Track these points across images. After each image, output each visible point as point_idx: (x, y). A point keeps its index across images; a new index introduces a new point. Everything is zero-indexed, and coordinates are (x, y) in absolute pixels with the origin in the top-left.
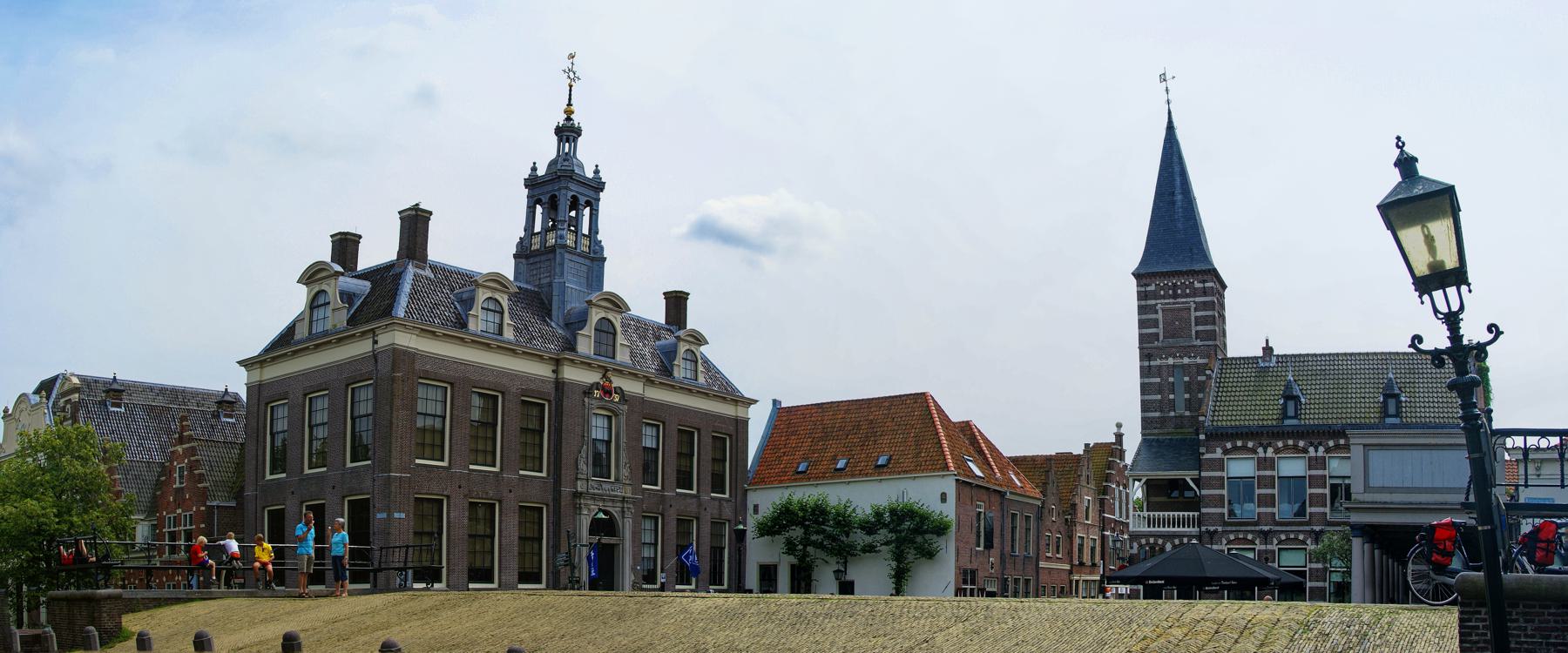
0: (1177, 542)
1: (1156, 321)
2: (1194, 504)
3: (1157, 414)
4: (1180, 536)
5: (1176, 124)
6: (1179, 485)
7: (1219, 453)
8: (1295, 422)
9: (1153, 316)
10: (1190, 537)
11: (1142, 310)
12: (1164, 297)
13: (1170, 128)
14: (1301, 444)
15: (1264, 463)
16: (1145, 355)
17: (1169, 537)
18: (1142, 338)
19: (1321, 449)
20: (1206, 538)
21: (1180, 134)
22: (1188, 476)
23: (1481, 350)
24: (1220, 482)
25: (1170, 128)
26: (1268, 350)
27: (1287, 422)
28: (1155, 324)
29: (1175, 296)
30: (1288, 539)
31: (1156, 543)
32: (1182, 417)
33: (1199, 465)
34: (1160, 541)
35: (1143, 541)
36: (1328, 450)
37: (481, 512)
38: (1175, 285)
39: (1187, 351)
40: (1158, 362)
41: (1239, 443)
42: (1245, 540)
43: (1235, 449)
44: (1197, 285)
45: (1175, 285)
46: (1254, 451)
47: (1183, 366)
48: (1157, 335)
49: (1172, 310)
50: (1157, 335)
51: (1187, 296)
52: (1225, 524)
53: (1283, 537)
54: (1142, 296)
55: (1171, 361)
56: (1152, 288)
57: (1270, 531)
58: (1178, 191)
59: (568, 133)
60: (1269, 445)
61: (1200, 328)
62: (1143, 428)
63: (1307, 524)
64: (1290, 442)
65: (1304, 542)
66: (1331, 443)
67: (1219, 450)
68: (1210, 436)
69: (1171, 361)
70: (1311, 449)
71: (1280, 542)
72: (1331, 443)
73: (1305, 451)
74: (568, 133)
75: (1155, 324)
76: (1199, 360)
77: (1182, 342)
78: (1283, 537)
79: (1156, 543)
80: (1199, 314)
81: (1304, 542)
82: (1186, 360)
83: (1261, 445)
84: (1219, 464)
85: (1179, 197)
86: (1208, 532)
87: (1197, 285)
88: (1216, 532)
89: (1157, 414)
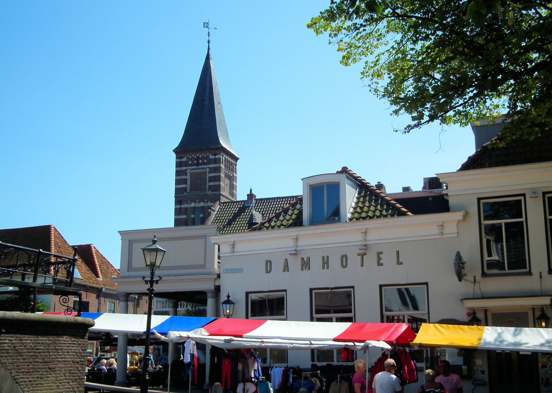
1: (186, 180)
5: (211, 56)
9: (184, 177)
11: (178, 173)
12: (191, 165)
13: (208, 58)
16: (178, 201)
18: (177, 191)
23: (391, 67)
25: (208, 58)
28: (185, 181)
29: (197, 164)
38: (198, 158)
44: (212, 157)
45: (198, 158)
51: (206, 164)
54: (178, 165)
55: (193, 205)
56: (184, 160)
59: (251, 190)
69: (193, 205)
74: (251, 190)
75: (185, 181)
77: (201, 193)
80: (211, 175)
85: (207, 102)
87: (212, 157)
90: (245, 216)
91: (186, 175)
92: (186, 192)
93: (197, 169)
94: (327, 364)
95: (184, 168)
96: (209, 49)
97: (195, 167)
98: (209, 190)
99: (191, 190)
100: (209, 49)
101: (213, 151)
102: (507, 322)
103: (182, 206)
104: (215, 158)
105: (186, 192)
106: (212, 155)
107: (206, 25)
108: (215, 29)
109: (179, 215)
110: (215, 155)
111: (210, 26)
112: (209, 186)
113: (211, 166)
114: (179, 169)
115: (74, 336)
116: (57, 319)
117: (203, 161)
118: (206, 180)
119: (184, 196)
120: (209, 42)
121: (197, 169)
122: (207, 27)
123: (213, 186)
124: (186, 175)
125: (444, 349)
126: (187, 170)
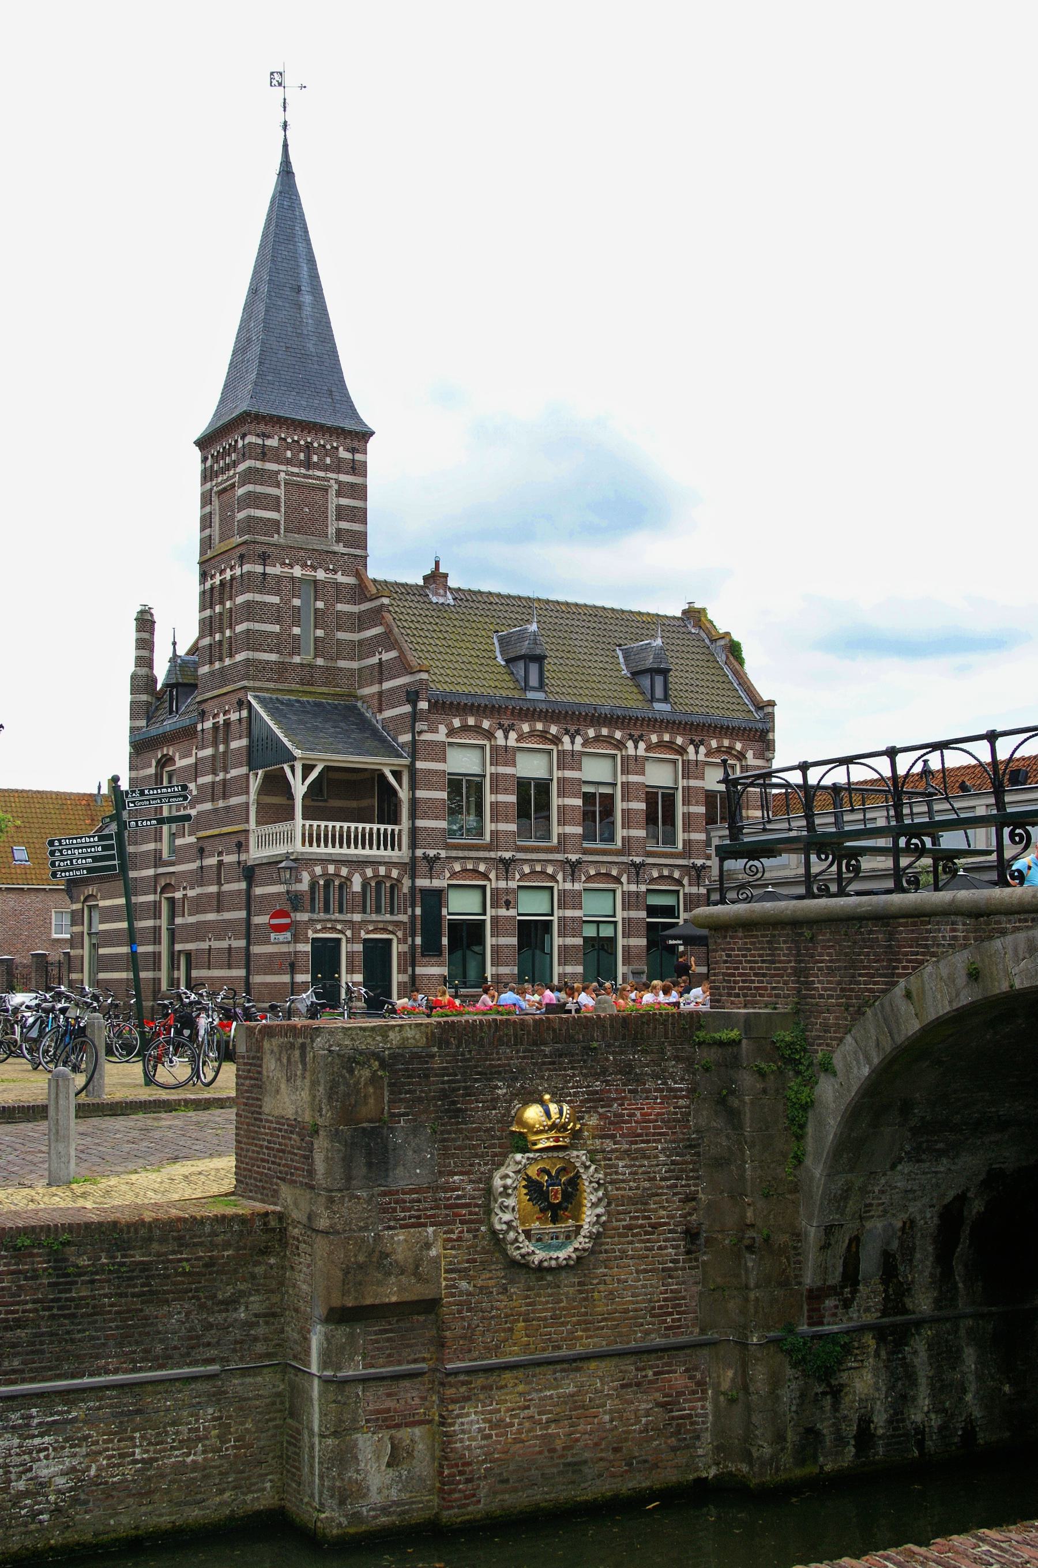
2: (389, 813)
3: (273, 657)
4: (375, 863)
5: (296, 168)
7: (441, 735)
8: (540, 696)
10: (389, 864)
12: (289, 462)
13: (286, 172)
14: (554, 730)
20: (422, 867)
25: (286, 172)
26: (436, 578)
27: (531, 695)
28: (342, 513)
29: (308, 464)
30: (533, 872)
34: (344, 871)
35: (382, 870)
37: (590, 815)
38: (308, 446)
39: (322, 558)
41: (471, 721)
44: (343, 454)
45: (308, 446)
49: (298, 485)
50: (277, 523)
51: (327, 468)
53: (527, 870)
56: (273, 442)
57: (513, 860)
59: (437, 563)
61: (344, 525)
63: (489, 848)
65: (617, 880)
66: (526, 728)
67: (443, 729)
73: (556, 740)
74: (437, 563)
75: (342, 513)
78: (527, 870)
86: (426, 857)
87: (343, 454)
88: (437, 858)
89: (273, 657)
94: (486, 978)
97: (303, 471)
98: (338, 541)
100: (285, 146)
101: (348, 441)
103: (269, 570)
107: (277, 79)
110: (353, 451)
113: (344, 478)
116: (842, 906)
122: (280, 84)
126: (278, 472)
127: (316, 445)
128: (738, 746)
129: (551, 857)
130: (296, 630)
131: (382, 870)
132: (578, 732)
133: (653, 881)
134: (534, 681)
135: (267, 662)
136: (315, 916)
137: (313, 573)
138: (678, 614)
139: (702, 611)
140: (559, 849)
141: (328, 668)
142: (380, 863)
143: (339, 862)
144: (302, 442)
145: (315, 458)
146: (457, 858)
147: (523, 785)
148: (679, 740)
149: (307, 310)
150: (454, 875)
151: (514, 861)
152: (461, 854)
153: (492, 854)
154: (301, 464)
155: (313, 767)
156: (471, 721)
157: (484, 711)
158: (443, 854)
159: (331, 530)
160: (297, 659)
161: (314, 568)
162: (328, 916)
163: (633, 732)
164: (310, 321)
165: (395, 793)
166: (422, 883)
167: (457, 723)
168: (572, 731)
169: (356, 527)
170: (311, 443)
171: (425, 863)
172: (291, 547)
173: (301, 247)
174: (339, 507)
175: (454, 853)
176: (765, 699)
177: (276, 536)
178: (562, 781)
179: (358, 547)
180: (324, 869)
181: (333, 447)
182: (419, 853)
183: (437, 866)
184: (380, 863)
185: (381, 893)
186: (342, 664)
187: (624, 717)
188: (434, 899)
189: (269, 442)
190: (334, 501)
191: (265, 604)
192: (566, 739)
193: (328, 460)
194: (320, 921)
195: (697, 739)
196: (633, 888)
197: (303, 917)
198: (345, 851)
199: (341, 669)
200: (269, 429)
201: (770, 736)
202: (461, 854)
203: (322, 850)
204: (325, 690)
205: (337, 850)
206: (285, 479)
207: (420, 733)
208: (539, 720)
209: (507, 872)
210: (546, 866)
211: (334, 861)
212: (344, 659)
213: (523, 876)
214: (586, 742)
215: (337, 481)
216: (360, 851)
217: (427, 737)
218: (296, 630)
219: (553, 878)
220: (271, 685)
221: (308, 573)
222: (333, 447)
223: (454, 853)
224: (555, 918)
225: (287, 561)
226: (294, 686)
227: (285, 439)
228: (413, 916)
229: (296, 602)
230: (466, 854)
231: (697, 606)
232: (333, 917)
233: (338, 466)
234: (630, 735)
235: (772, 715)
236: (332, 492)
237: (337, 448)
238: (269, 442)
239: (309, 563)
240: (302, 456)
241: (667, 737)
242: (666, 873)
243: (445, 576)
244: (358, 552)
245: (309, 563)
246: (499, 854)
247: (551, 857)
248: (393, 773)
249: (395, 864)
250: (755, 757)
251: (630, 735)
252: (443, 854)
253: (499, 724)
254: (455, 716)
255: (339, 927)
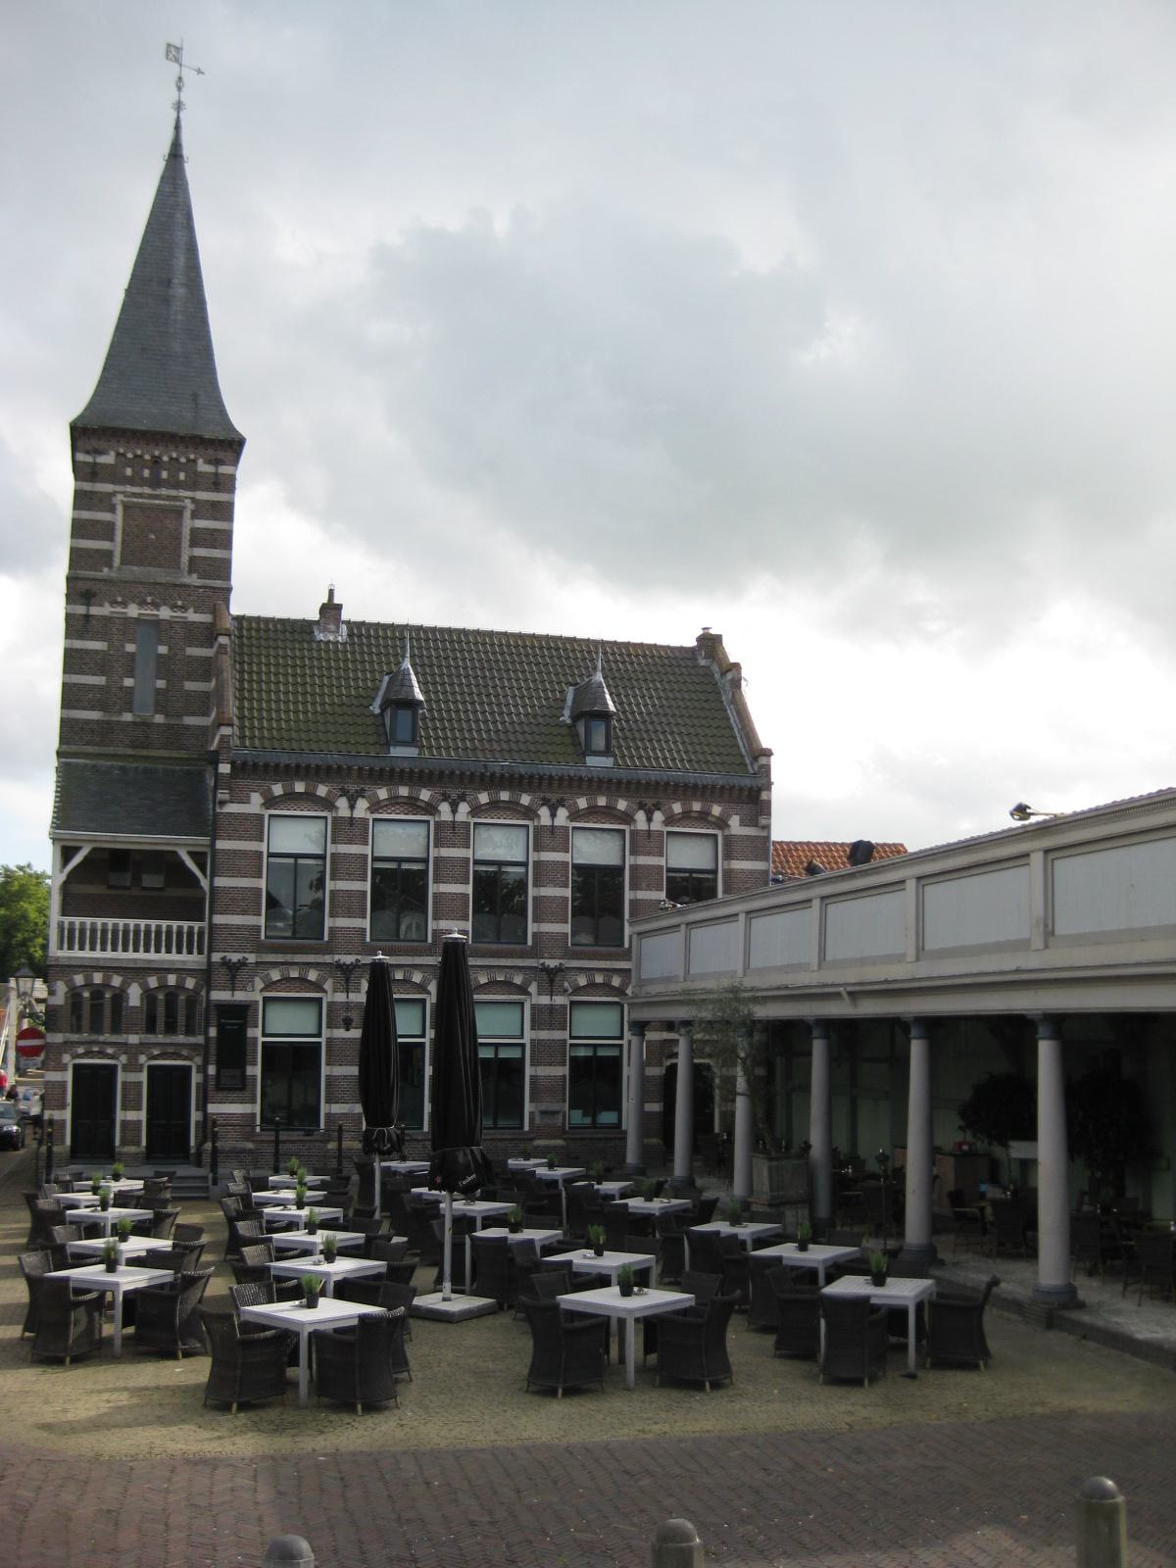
0: (153, 982)
2: (192, 909)
3: (94, 715)
4: (162, 971)
5: (187, 151)
6: (167, 863)
7: (255, 804)
8: (412, 752)
12: (131, 481)
13: (175, 156)
14: (425, 795)
15: (544, 838)
17: (137, 972)
19: (658, 816)
20: (220, 976)
21: (191, 170)
22: (183, 846)
24: (251, 863)
25: (175, 156)
26: (331, 609)
28: (107, 530)
29: (155, 482)
31: (106, 985)
32: (145, 725)
33: (212, 827)
35: (79, 980)
36: (476, 810)
39: (168, 593)
40: (106, 610)
42: (508, 985)
43: (290, 797)
44: (203, 467)
45: (156, 461)
46: (328, 804)
47: (157, 623)
48: (109, 554)
50: (109, 554)
51: (178, 485)
52: (260, 948)
56: (108, 459)
57: (560, 969)
58: (178, 279)
59: (331, 593)
60: (361, 794)
61: (200, 552)
62: (64, 739)
64: (404, 791)
65: (523, 990)
66: (677, 808)
67: (256, 799)
68: (240, 769)
69: (133, 611)
70: (445, 807)
71: (270, 985)
72: (677, 808)
74: (331, 593)
75: (198, 538)
76: (192, 616)
79: (106, 985)
81: (317, 986)
82: (165, 613)
83: (344, 793)
84: (254, 827)
86: (225, 963)
87: (203, 467)
88: (243, 964)
89: (94, 715)
90: (1053, 863)
91: (112, 509)
92: (110, 566)
93: (151, 497)
95: (108, 488)
96: (177, 127)
97: (147, 490)
98: (190, 572)
99: (123, 562)
100: (177, 127)
102: (89, 1291)
103: (95, 611)
104: (216, 474)
105: (110, 566)
106: (209, 462)
107: (174, 53)
108: (199, 72)
109: (82, 638)
110: (217, 462)
111: (185, 59)
112: (192, 559)
113: (202, 495)
114: (87, 486)
115: (147, 1024)
117: (173, 475)
118: (178, 538)
119: (104, 581)
120: (179, 106)
121: (151, 497)
123: (205, 558)
124: (112, 509)
125: (855, 869)
126: (114, 494)
127: (165, 459)
128: (716, 810)
129: (419, 960)
130: (128, 682)
131: (172, 980)
132: (462, 797)
133: (577, 990)
134: (404, 733)
135: (87, 722)
136: (152, 1038)
137: (184, 615)
138: (693, 643)
139: (718, 639)
140: (535, 952)
141: (170, 727)
142: (169, 971)
143: (108, 969)
144: (147, 457)
145: (164, 475)
146: (581, 970)
147: (584, 871)
148: (622, 805)
149: (177, 306)
150: (270, 985)
151: (359, 967)
152: (280, 958)
153: (328, 959)
154: (143, 482)
155: (77, 849)
156: (300, 787)
157: (580, 786)
158: (252, 958)
159: (185, 559)
160: (128, 717)
161: (156, 606)
162: (94, 1037)
163: (548, 795)
164: (180, 317)
165: (197, 880)
166: (220, 996)
167: (278, 789)
168: (454, 796)
169: (216, 553)
170: (159, 457)
171: (224, 970)
172: (126, 582)
173: (180, 237)
174: (194, 531)
175: (271, 958)
176: (764, 747)
177: (106, 570)
178: (634, 868)
179: (219, 578)
180: (107, 978)
181: (189, 460)
182: (216, 957)
183: (243, 974)
184: (169, 971)
185: (168, 1010)
186: (189, 720)
187: (531, 777)
188: (237, 1016)
189: (102, 459)
190: (188, 524)
191: (87, 652)
192: (445, 807)
193: (182, 476)
194: (81, 1043)
195: (649, 802)
196: (545, 1000)
197: (57, 1038)
198: (120, 955)
199: (187, 727)
200: (102, 444)
201: (764, 796)
202: (280, 958)
203: (87, 954)
204: (165, 753)
205: (109, 954)
206: (122, 501)
207: (223, 803)
208: (402, 783)
209: (347, 980)
210: (411, 973)
211: (102, 968)
212: (193, 714)
213: (577, 990)
214: (670, 820)
215: (193, 500)
216: (141, 955)
217: (232, 808)
218: (128, 682)
219: (317, 986)
220: (90, 749)
221: (149, 612)
222: (189, 460)
223: (271, 958)
224: (323, 1040)
225: (119, 599)
226: (121, 751)
227: (123, 455)
228: (207, 1039)
229: (130, 648)
230: (289, 958)
231: (712, 632)
232: (101, 1038)
233: (195, 482)
234: (544, 799)
235: (767, 769)
236: (187, 514)
237: (194, 461)
238: (102, 459)
239: (149, 599)
240: (146, 473)
241: (602, 801)
242: (599, 979)
243: (339, 607)
244: (218, 583)
245: (149, 599)
246: (337, 957)
247: (419, 960)
248: (191, 854)
249: (191, 972)
250: (743, 823)
251: (544, 799)
252: (252, 958)
253: (342, 789)
254: (277, 781)
255: (110, 1051)
